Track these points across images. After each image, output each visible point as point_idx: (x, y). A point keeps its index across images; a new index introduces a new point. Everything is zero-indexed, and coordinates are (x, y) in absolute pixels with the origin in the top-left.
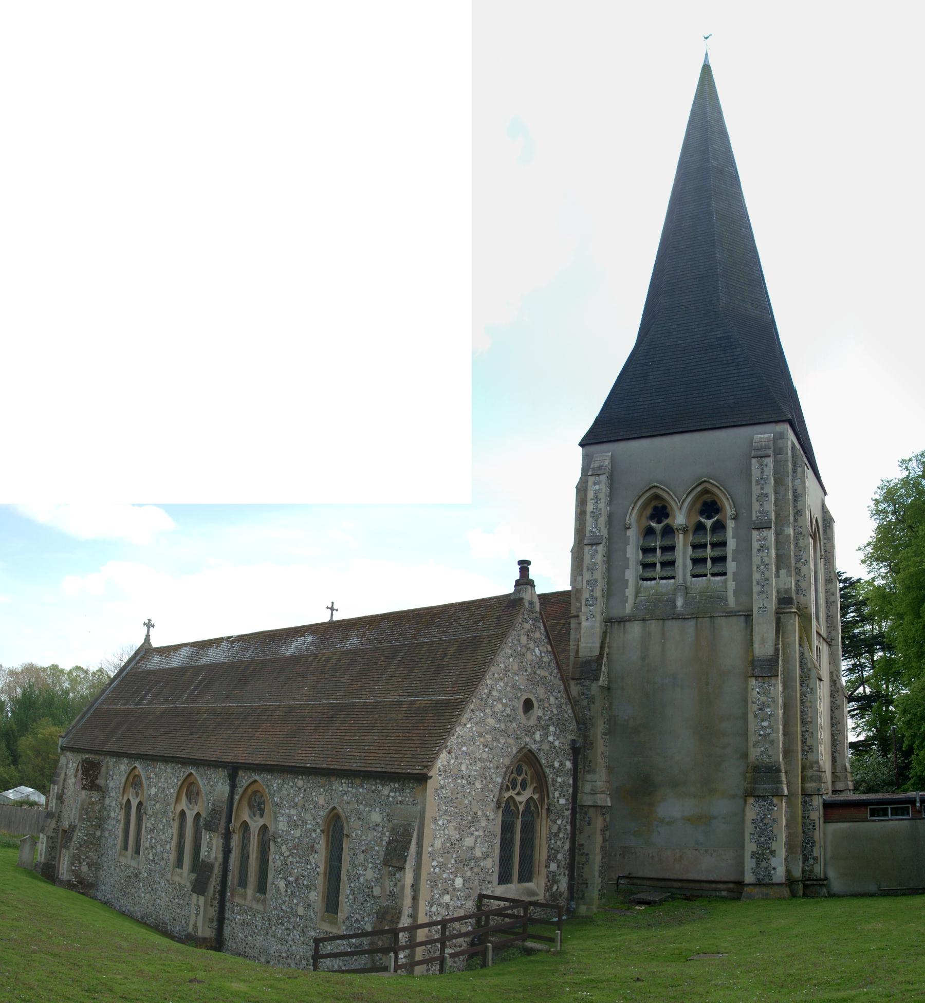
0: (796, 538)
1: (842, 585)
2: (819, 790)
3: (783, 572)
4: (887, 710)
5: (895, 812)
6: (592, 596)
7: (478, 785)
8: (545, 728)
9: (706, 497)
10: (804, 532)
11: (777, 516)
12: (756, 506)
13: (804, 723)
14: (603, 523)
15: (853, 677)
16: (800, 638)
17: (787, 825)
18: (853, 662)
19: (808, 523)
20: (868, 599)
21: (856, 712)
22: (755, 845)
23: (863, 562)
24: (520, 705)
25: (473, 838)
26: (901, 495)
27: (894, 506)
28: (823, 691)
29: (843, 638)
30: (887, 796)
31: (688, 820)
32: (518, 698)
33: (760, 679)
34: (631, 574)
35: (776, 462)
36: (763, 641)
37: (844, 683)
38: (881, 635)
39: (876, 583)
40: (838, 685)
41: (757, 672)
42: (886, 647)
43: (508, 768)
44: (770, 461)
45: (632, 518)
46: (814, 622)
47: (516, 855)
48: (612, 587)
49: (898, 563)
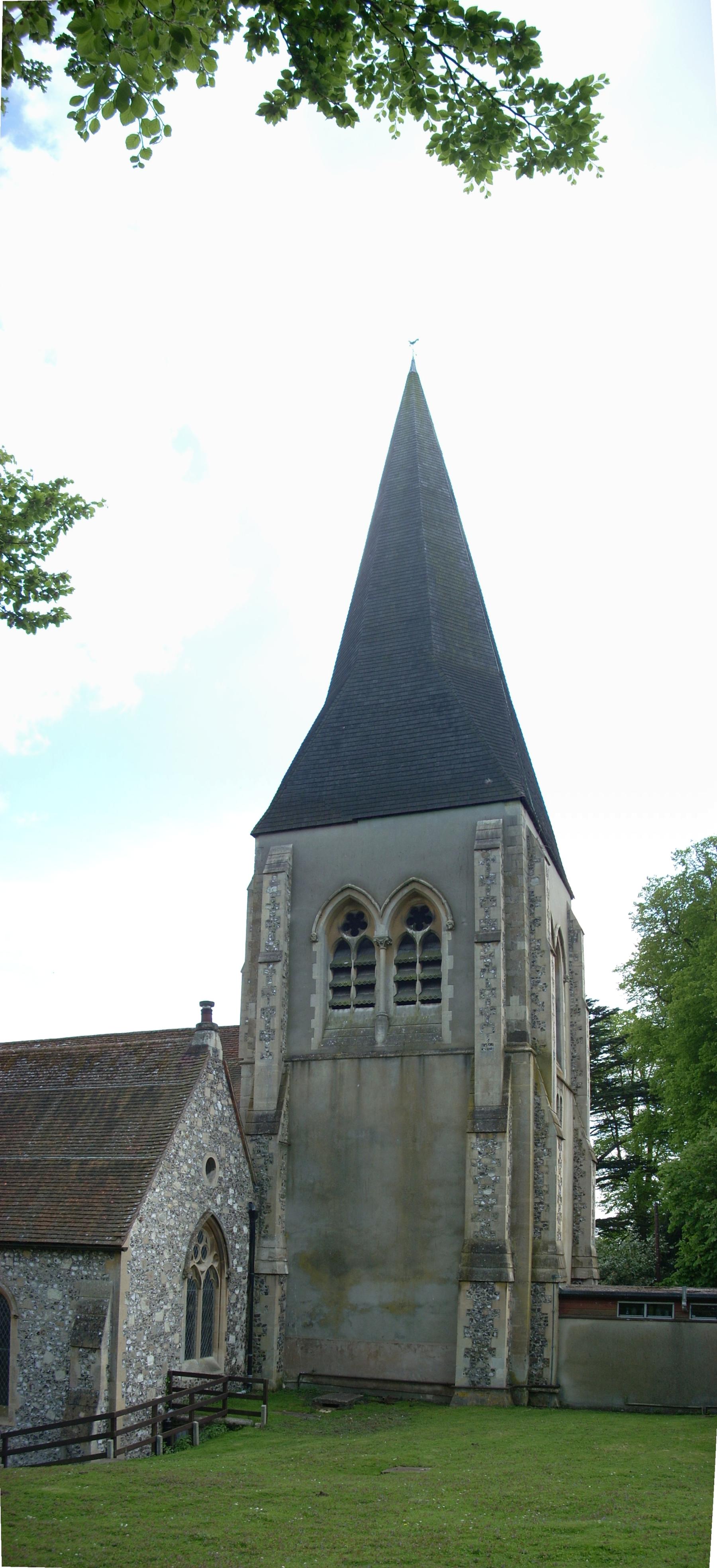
0: (532, 955)
1: (592, 1017)
2: (554, 1277)
3: (515, 999)
4: (648, 1181)
5: (653, 1310)
6: (268, 1028)
7: (166, 1256)
8: (225, 1190)
9: (415, 902)
10: (543, 947)
11: (508, 925)
12: (480, 914)
13: (538, 1192)
14: (282, 934)
15: (605, 1136)
16: (536, 1085)
17: (511, 1319)
18: (605, 1117)
19: (549, 936)
20: (627, 1036)
21: (606, 1181)
22: (470, 1341)
23: (622, 987)
24: (203, 1165)
25: (162, 1312)
26: (675, 899)
27: (666, 912)
28: (564, 1153)
29: (592, 1085)
30: (643, 1290)
31: (386, 1307)
32: (202, 1158)
33: (482, 1136)
34: (318, 1001)
35: (507, 856)
36: (487, 1087)
37: (592, 1144)
38: (644, 1083)
39: (639, 1015)
40: (584, 1146)
41: (478, 1126)
42: (652, 1099)
43: (193, 1235)
44: (498, 855)
45: (320, 928)
46: (555, 1064)
47: (200, 1333)
48: (294, 1016)
49: (669, 988)
